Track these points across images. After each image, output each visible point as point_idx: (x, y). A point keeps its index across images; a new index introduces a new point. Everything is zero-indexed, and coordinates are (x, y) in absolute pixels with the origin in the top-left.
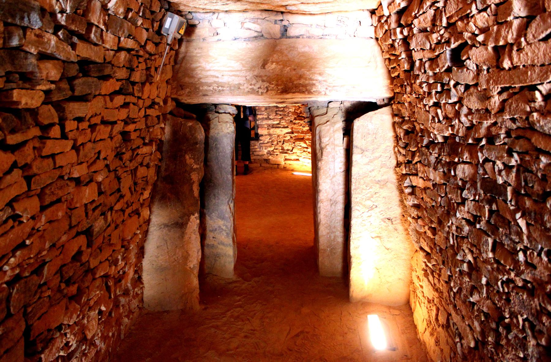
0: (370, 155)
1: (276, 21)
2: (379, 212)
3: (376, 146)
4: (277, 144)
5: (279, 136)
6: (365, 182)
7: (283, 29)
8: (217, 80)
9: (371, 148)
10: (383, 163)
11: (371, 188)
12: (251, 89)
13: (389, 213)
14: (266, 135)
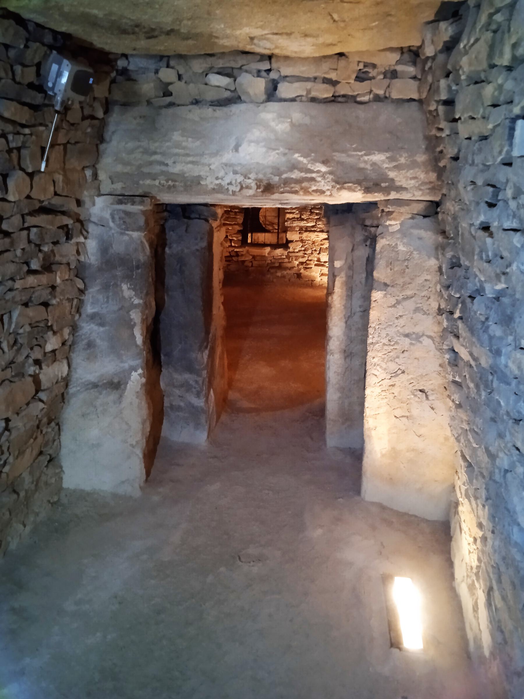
0: (398, 293)
1: (259, 71)
2: (408, 380)
3: (407, 279)
4: (312, 253)
5: (314, 243)
6: (387, 335)
7: (271, 85)
8: (164, 168)
9: (400, 281)
10: (418, 305)
11: (397, 343)
12: (217, 185)
13: (422, 383)
14: (296, 241)
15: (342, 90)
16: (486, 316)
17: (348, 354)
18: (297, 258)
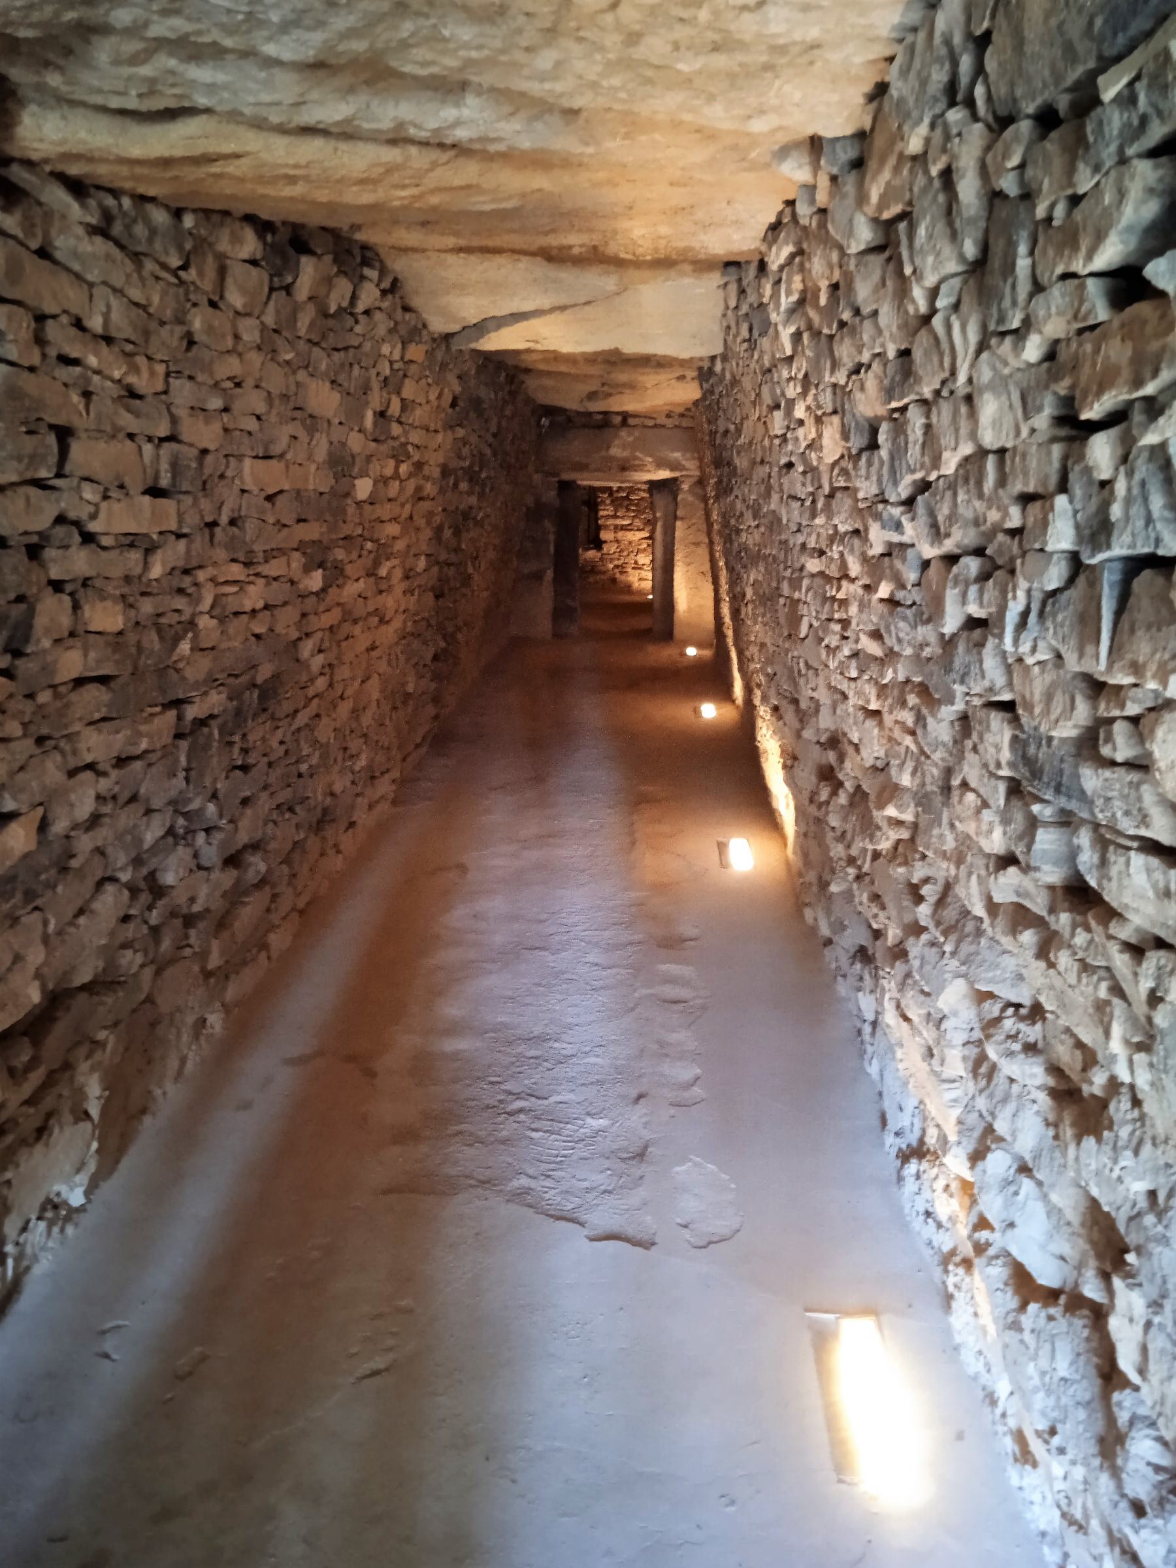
15: (659, 422)
16: (1040, 1045)
17: (665, 533)
18: (612, 560)
